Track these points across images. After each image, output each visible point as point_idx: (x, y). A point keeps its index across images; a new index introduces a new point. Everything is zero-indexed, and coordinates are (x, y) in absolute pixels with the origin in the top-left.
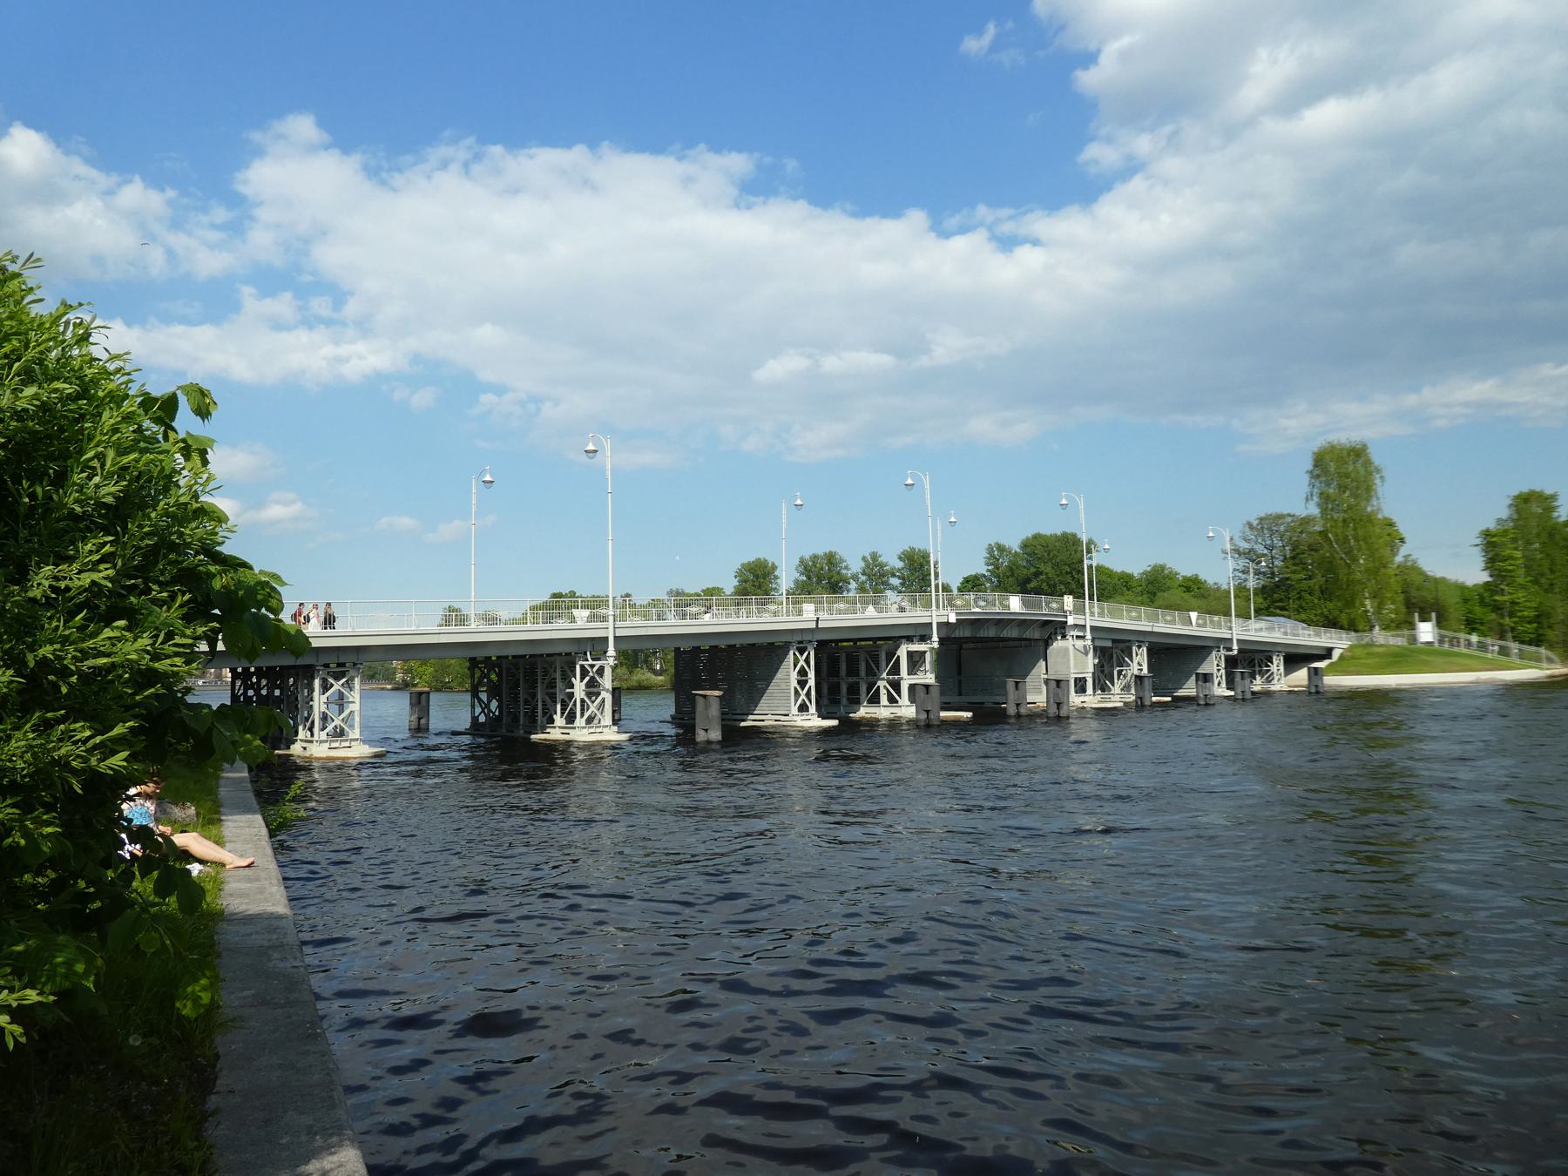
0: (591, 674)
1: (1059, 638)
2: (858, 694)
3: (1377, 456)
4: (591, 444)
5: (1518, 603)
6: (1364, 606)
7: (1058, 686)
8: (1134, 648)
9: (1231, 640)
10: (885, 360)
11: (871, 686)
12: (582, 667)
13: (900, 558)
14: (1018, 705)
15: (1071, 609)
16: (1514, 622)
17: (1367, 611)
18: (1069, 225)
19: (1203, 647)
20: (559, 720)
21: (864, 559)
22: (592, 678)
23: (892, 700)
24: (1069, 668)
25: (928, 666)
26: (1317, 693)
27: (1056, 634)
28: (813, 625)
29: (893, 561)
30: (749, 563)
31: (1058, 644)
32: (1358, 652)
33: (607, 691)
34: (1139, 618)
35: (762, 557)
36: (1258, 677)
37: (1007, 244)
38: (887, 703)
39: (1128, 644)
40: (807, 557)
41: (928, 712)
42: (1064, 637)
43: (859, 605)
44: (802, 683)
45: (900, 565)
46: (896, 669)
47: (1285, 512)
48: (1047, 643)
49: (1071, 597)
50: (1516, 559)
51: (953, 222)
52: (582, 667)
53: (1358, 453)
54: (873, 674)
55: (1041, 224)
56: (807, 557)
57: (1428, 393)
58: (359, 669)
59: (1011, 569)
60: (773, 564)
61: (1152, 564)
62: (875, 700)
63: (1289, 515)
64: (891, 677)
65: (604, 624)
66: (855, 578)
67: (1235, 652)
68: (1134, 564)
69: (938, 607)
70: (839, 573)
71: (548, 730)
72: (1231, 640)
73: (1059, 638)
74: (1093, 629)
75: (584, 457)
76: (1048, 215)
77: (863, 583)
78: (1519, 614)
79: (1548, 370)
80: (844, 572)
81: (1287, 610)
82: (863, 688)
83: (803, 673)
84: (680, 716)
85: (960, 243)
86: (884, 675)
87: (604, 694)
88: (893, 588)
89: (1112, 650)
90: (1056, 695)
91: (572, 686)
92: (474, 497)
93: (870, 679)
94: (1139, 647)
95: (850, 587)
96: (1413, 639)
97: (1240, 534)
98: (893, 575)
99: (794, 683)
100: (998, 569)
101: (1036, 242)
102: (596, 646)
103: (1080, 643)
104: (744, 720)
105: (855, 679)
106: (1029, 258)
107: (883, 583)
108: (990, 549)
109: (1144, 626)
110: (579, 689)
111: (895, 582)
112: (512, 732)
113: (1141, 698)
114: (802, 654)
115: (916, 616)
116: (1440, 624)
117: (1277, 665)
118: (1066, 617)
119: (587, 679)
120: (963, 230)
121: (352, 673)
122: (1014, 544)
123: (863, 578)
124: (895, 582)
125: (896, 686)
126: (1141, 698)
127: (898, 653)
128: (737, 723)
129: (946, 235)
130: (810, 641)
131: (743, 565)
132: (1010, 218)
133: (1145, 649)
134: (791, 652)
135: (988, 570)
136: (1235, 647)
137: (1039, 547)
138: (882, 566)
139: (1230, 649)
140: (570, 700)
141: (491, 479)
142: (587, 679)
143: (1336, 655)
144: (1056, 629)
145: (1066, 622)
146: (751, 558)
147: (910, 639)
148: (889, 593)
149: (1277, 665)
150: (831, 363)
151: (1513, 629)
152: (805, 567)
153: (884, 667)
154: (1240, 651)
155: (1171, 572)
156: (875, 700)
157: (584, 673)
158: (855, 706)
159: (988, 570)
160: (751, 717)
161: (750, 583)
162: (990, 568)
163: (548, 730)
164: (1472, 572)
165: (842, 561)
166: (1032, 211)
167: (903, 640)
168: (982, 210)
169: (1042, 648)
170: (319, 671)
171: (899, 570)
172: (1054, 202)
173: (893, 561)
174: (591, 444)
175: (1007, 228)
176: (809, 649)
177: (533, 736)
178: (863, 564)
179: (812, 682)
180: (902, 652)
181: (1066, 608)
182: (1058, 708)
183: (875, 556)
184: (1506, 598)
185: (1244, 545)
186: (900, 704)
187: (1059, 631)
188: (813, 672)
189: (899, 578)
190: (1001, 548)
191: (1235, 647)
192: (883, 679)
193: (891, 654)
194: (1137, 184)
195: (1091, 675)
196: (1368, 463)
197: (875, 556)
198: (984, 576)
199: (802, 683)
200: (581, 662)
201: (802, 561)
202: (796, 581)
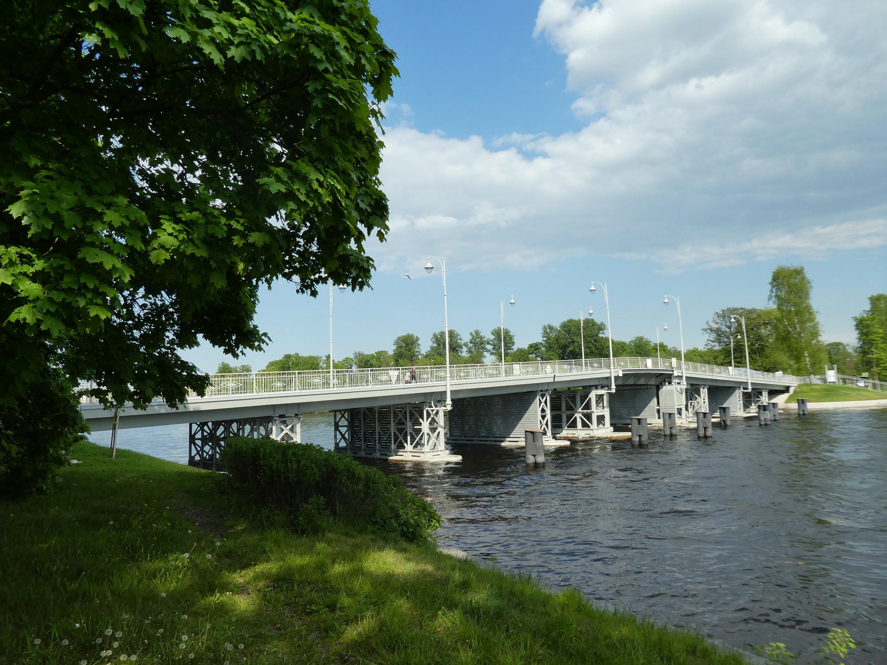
0: (432, 416)
1: (667, 384)
2: (561, 421)
3: (809, 274)
4: (429, 263)
5: (882, 359)
6: (805, 361)
7: (704, 417)
8: (701, 389)
9: (747, 383)
10: (449, 221)
11: (569, 417)
12: (427, 411)
13: (492, 334)
14: (671, 428)
15: (675, 366)
16: (880, 370)
17: (806, 365)
18: (565, 145)
19: (728, 387)
20: (409, 447)
21: (471, 334)
22: (433, 418)
23: (585, 425)
24: (674, 402)
25: (605, 404)
26: (804, 414)
27: (665, 381)
28: (552, 380)
29: (488, 335)
30: (402, 337)
31: (666, 389)
32: (805, 389)
33: (441, 427)
34: (705, 371)
35: (410, 333)
36: (753, 404)
37: (529, 156)
38: (581, 428)
39: (697, 387)
40: (438, 333)
41: (640, 436)
42: (670, 383)
43: (574, 366)
44: (543, 417)
45: (492, 337)
46: (588, 406)
47: (739, 307)
48: (658, 388)
49: (675, 359)
50: (879, 333)
51: (499, 142)
52: (427, 411)
53: (798, 272)
54: (571, 409)
55: (549, 145)
56: (438, 333)
57: (755, 243)
58: (300, 418)
59: (557, 340)
60: (417, 337)
61: (636, 336)
62: (573, 425)
63: (741, 309)
64: (585, 411)
65: (443, 383)
66: (466, 345)
67: (750, 390)
68: (627, 337)
69: (614, 366)
70: (456, 342)
71: (400, 454)
72: (747, 383)
73: (667, 384)
74: (687, 378)
75: (425, 272)
76: (553, 140)
77: (471, 348)
78: (882, 365)
79: (818, 230)
80: (459, 341)
81: (742, 364)
82: (564, 418)
83: (543, 411)
84: (453, 438)
85: (502, 156)
86: (580, 410)
87: (439, 429)
88: (488, 351)
89: (693, 390)
90: (704, 422)
91: (420, 424)
92: (331, 298)
93: (570, 412)
94: (704, 388)
95: (462, 350)
96: (825, 380)
97: (712, 320)
98: (488, 343)
99: (540, 418)
100: (549, 339)
101: (545, 155)
102: (439, 397)
103: (679, 387)
104: (502, 441)
105: (559, 412)
106: (541, 164)
107: (482, 348)
108: (545, 328)
109: (708, 375)
110: (425, 426)
111: (489, 347)
112: (357, 453)
113: (724, 421)
114: (543, 398)
115: (602, 373)
116: (840, 371)
117: (765, 394)
118: (673, 371)
119: (430, 419)
120: (505, 147)
121: (295, 420)
122: (557, 325)
123: (471, 345)
124: (489, 347)
125: (589, 417)
126: (724, 421)
127: (590, 396)
128: (498, 443)
129: (496, 150)
130: (547, 390)
131: (399, 338)
132: (531, 140)
133: (706, 389)
134: (538, 397)
135: (543, 340)
136: (750, 387)
137: (573, 327)
138: (481, 338)
139: (747, 389)
140: (418, 434)
141: (594, 289)
142: (430, 419)
143: (792, 390)
144: (665, 378)
145: (673, 374)
146: (403, 333)
147: (596, 388)
148: (485, 354)
149: (765, 394)
150: (422, 223)
151: (879, 374)
152: (437, 339)
153: (579, 403)
154: (753, 389)
155: (646, 341)
156: (573, 425)
157: (429, 415)
158: (559, 430)
159: (543, 340)
160: (508, 439)
161: (404, 348)
162: (545, 339)
163: (400, 454)
164: (850, 339)
165: (458, 335)
166: (542, 137)
167: (594, 388)
168: (515, 136)
169: (655, 390)
170: (276, 420)
171: (492, 341)
172: (556, 132)
173: (488, 335)
174: (429, 263)
175: (530, 146)
176: (546, 394)
177: (391, 458)
178: (470, 337)
179: (549, 417)
180: (593, 395)
181: (673, 366)
182: (705, 431)
183: (477, 333)
184: (875, 356)
185: (715, 326)
186: (591, 428)
187: (667, 380)
188: (549, 410)
189: (492, 345)
190: (551, 328)
191: (750, 387)
192: (579, 412)
193: (585, 396)
194: (602, 123)
195: (684, 406)
196: (803, 278)
197: (477, 333)
198: (541, 344)
199: (543, 417)
200: (427, 409)
201: (435, 335)
202: (432, 348)
